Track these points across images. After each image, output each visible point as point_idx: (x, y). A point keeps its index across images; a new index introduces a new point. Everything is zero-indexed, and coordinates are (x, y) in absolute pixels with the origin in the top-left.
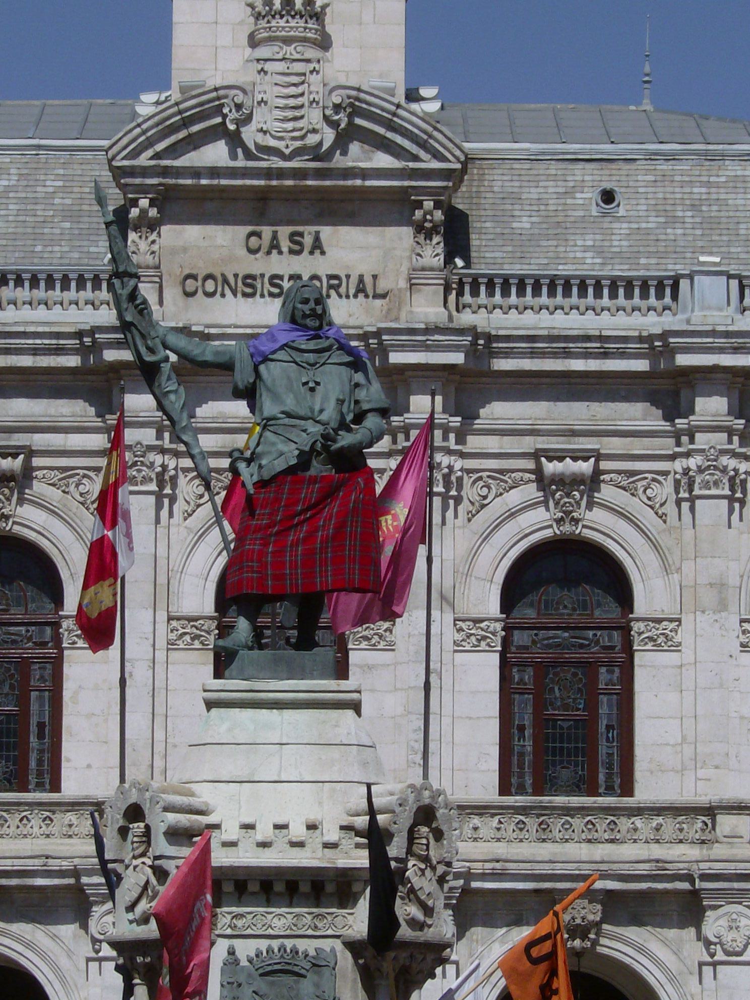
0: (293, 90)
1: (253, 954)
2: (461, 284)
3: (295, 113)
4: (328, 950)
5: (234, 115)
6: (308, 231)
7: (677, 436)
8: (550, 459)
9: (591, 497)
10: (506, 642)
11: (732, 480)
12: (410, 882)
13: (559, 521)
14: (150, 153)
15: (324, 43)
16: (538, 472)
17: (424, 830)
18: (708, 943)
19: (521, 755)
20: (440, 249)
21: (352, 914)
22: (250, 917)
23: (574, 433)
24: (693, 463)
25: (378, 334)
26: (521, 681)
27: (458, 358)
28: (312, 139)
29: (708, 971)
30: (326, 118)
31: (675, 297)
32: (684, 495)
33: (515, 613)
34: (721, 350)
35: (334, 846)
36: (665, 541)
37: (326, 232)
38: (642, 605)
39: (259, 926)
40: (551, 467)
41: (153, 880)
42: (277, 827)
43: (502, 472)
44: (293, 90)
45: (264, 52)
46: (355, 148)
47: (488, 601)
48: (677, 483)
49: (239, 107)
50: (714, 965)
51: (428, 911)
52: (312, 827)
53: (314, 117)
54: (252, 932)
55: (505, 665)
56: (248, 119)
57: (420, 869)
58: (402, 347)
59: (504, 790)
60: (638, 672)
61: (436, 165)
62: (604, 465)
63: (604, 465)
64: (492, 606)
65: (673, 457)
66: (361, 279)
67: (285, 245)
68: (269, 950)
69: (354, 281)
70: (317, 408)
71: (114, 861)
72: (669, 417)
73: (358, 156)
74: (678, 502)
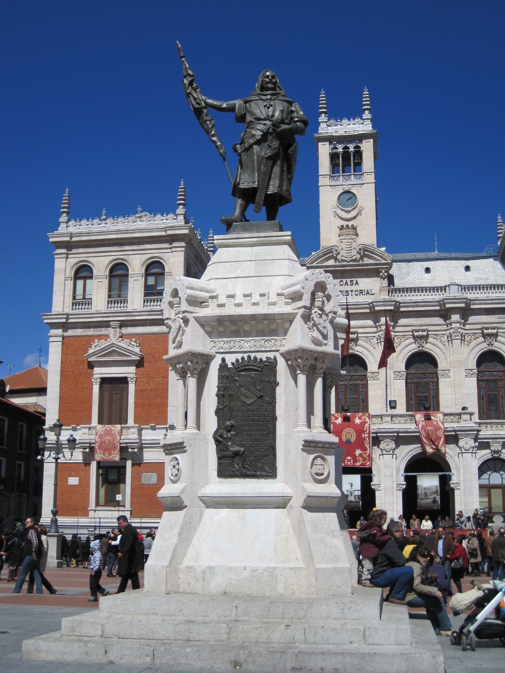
0: (349, 246)
1: (234, 361)
2: (392, 291)
3: (350, 250)
4: (273, 358)
5: (335, 252)
6: (354, 280)
7: (447, 325)
8: (416, 332)
9: (426, 341)
10: (406, 377)
11: (461, 335)
12: (313, 320)
13: (419, 347)
14: (316, 263)
15: (357, 235)
16: (413, 335)
17: (320, 294)
18: (460, 448)
19: (412, 405)
20: (387, 282)
21: (285, 339)
22: (232, 343)
23: (422, 326)
24: (451, 331)
25: (372, 303)
26: (411, 387)
27: (392, 308)
28: (354, 258)
29: (460, 455)
30: (358, 252)
31: (445, 291)
32: (450, 339)
33: (409, 370)
34: (457, 303)
35: (274, 304)
36: (445, 351)
37: (359, 280)
38: (440, 367)
39: (237, 347)
40: (416, 334)
41: (183, 325)
42: (245, 296)
43: (404, 336)
44: (349, 246)
45: (342, 237)
46: (365, 259)
47: (402, 367)
48: (448, 336)
49: (336, 250)
50: (462, 453)
51: (325, 337)
52: (262, 295)
53: (354, 252)
54: (233, 350)
55: (406, 382)
56: (339, 253)
57: (319, 314)
58: (378, 306)
59: (407, 411)
60: (440, 383)
61: (383, 261)
62: (429, 333)
63: (429, 333)
64: (403, 368)
65: (446, 330)
66: (368, 290)
67: (349, 283)
68: (243, 358)
69: (366, 291)
70: (270, 114)
71: (167, 319)
72: (445, 321)
73: (367, 261)
74: (448, 341)
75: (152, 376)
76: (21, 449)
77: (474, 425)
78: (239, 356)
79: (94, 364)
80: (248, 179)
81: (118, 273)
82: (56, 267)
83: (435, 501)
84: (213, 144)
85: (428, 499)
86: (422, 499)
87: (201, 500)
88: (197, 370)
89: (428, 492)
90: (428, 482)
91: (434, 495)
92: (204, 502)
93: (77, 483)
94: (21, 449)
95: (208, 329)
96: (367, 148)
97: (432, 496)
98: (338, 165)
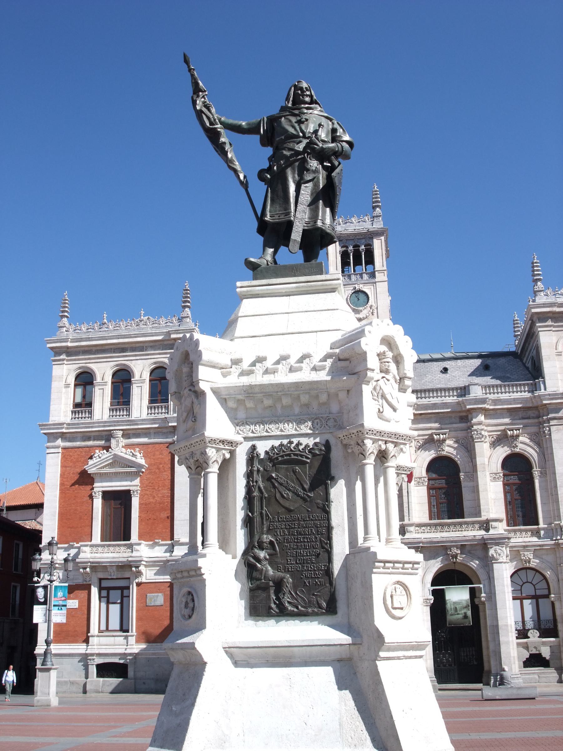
59: (431, 518)
64: (424, 474)
75: (156, 488)
76: (16, 569)
77: (503, 532)
78: (277, 443)
79: (94, 476)
80: (279, 211)
81: (122, 381)
82: (54, 374)
83: (466, 617)
84: (232, 173)
85: (458, 614)
86: (452, 615)
87: (227, 652)
88: (218, 462)
89: (458, 607)
90: (457, 596)
91: (465, 610)
92: (231, 656)
93: (77, 606)
94: (16, 569)
95: (231, 404)
96: (378, 246)
97: (463, 612)
98: (349, 264)
